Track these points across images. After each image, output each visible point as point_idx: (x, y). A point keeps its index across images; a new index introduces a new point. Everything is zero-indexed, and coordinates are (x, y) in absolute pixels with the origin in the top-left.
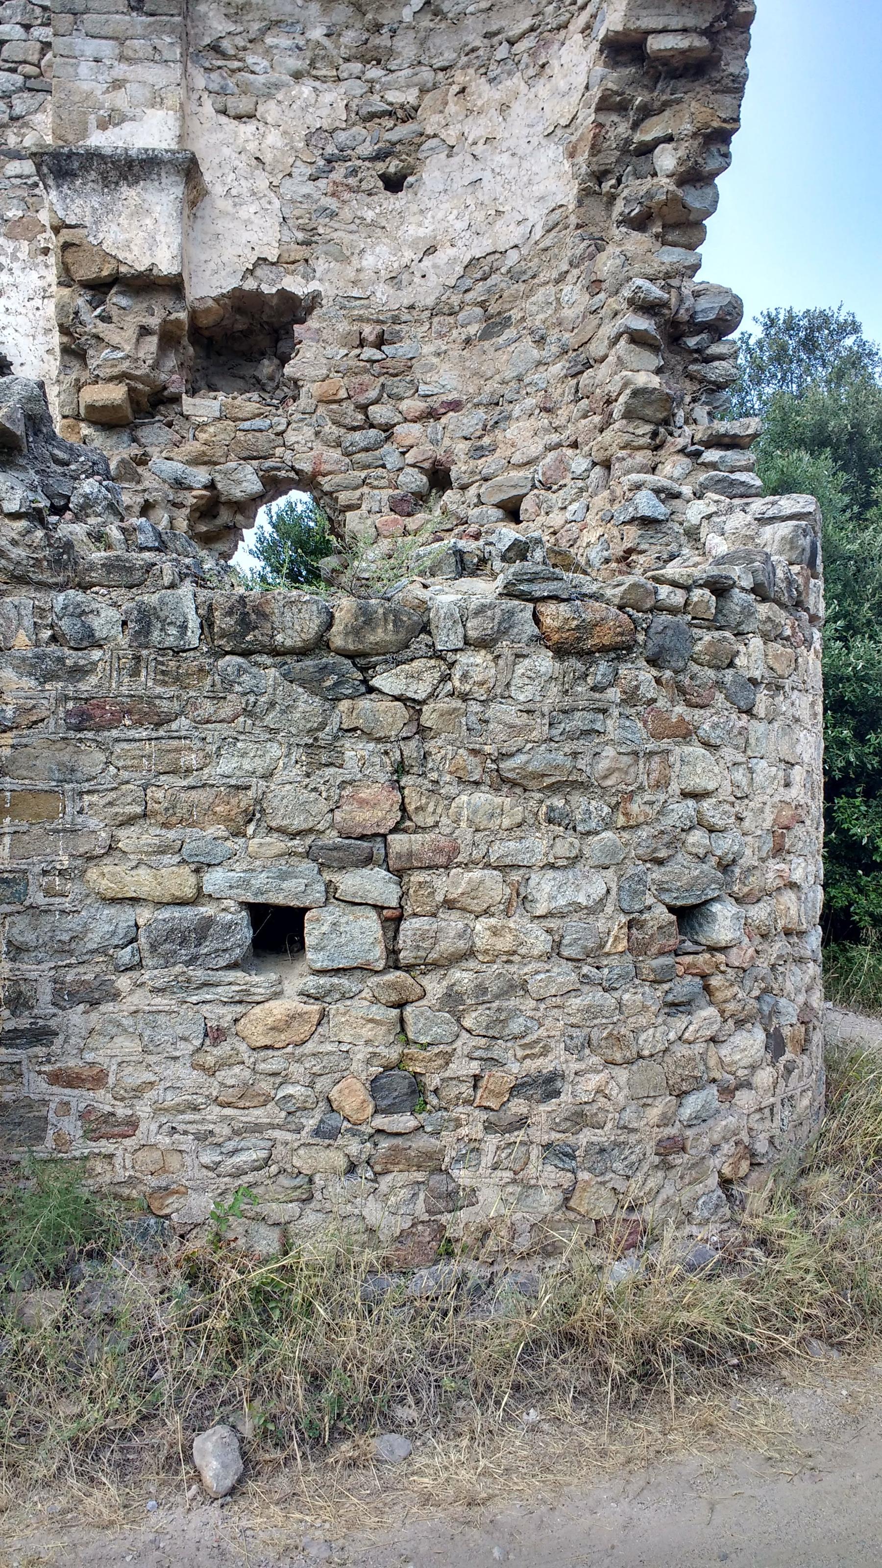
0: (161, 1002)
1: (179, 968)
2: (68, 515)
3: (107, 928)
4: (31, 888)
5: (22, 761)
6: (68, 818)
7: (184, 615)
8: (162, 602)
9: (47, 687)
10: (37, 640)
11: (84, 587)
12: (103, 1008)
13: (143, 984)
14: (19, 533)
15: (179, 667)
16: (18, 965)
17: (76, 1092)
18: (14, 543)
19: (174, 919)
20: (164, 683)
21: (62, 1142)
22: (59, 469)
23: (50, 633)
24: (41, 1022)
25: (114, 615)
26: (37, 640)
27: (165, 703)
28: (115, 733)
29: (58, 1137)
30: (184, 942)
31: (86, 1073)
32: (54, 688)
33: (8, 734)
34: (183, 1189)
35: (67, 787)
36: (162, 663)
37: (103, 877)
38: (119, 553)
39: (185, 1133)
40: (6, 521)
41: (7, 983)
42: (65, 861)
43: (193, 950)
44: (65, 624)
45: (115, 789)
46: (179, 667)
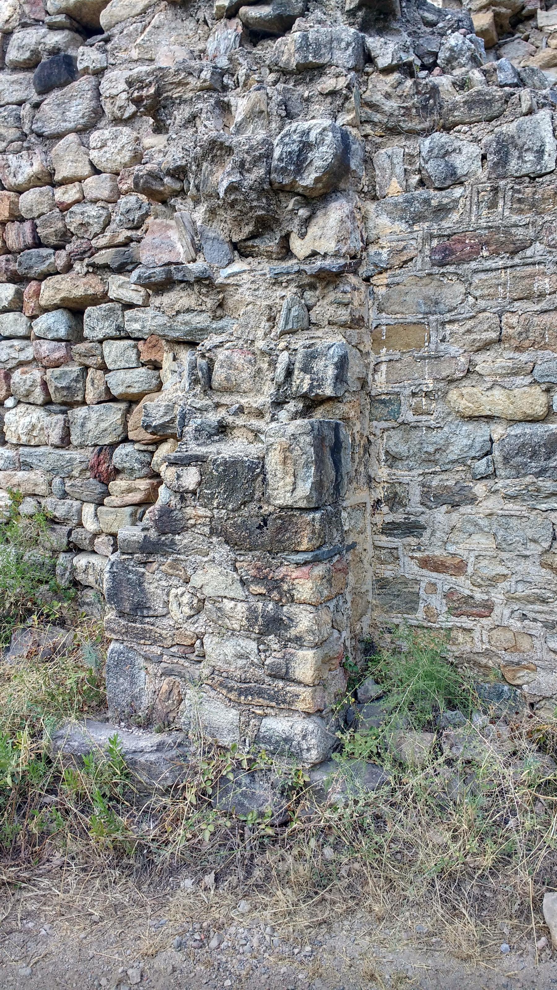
0: (512, 507)
1: (529, 479)
2: (437, 70)
3: (466, 442)
4: (403, 408)
5: (395, 297)
6: (432, 346)
7: (542, 140)
8: (520, 130)
9: (416, 228)
10: (407, 186)
11: (447, 129)
12: (462, 509)
13: (497, 491)
14: (392, 86)
15: (534, 193)
16: (394, 471)
17: (441, 576)
18: (388, 96)
19: (525, 434)
20: (520, 211)
21: (430, 614)
22: (429, 30)
23: (418, 177)
24: (413, 518)
25: (475, 150)
26: (407, 186)
27: (521, 231)
28: (473, 265)
29: (428, 609)
30: (534, 455)
31: (449, 562)
32: (421, 228)
33: (385, 275)
34: (533, 666)
35: (432, 318)
36: (519, 191)
37: (462, 398)
38: (480, 88)
39: (535, 620)
40: (381, 77)
41: (386, 485)
42: (431, 385)
43: (543, 463)
44: (432, 168)
45: (473, 317)
46: (534, 193)
